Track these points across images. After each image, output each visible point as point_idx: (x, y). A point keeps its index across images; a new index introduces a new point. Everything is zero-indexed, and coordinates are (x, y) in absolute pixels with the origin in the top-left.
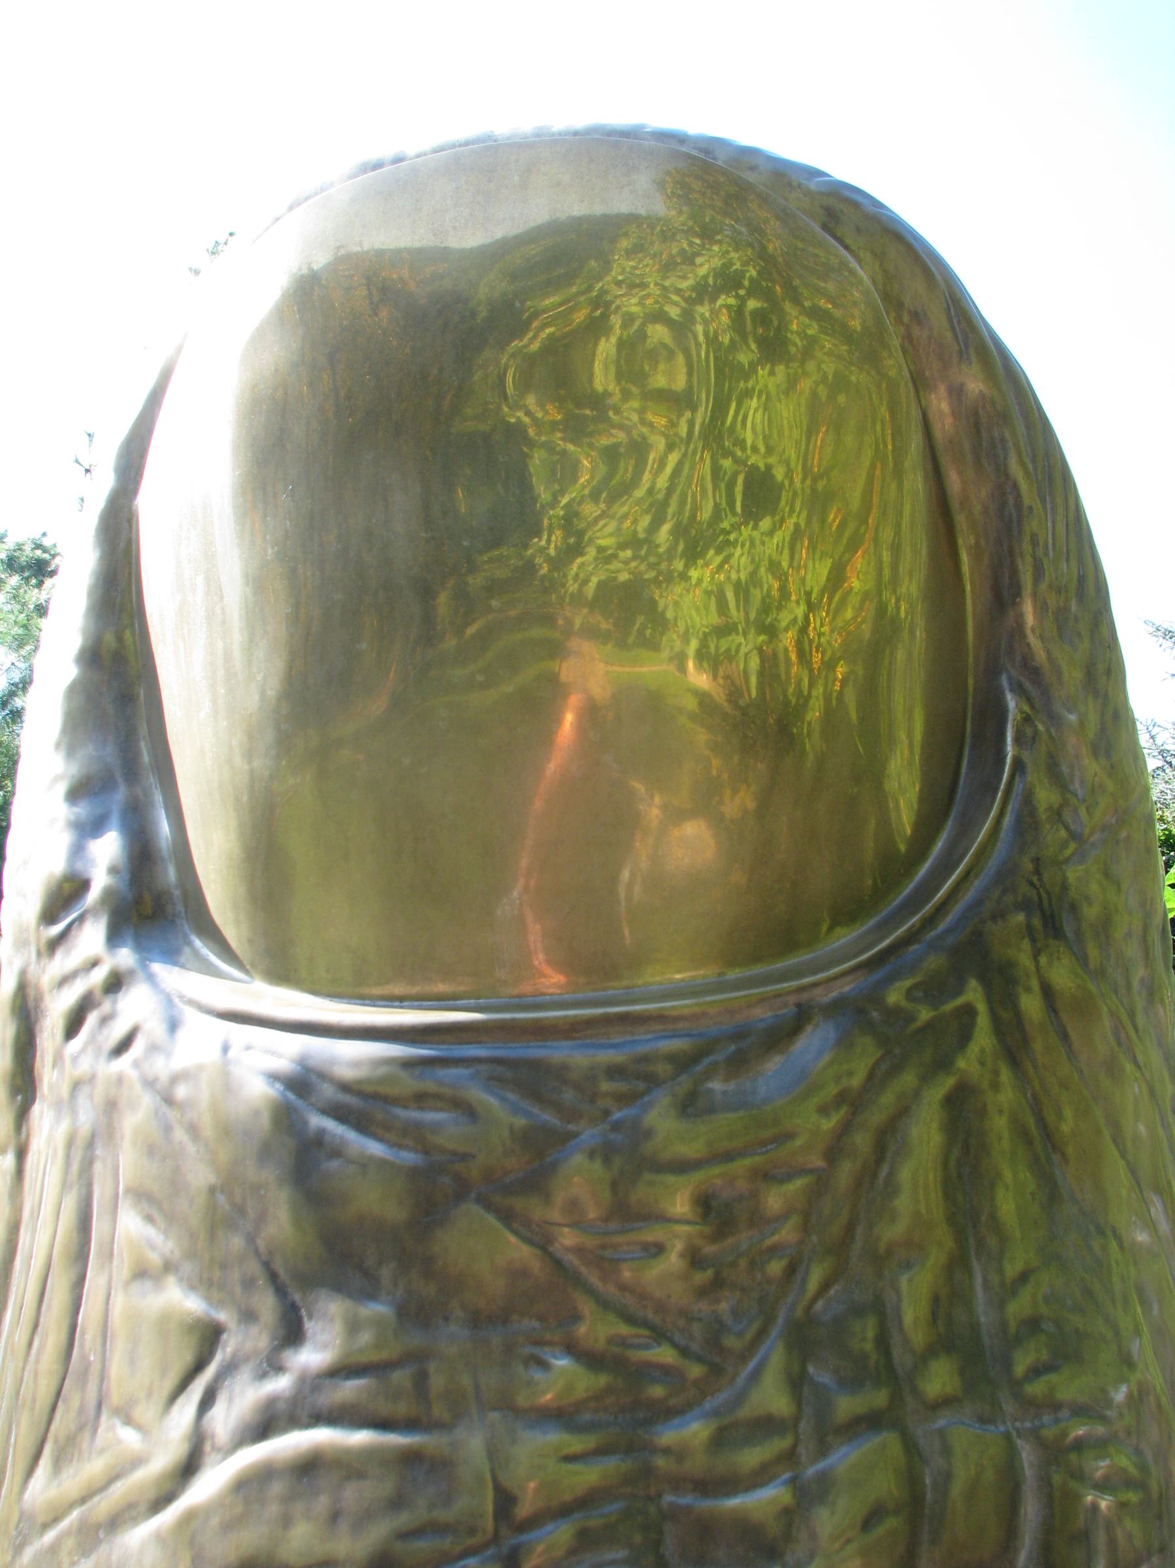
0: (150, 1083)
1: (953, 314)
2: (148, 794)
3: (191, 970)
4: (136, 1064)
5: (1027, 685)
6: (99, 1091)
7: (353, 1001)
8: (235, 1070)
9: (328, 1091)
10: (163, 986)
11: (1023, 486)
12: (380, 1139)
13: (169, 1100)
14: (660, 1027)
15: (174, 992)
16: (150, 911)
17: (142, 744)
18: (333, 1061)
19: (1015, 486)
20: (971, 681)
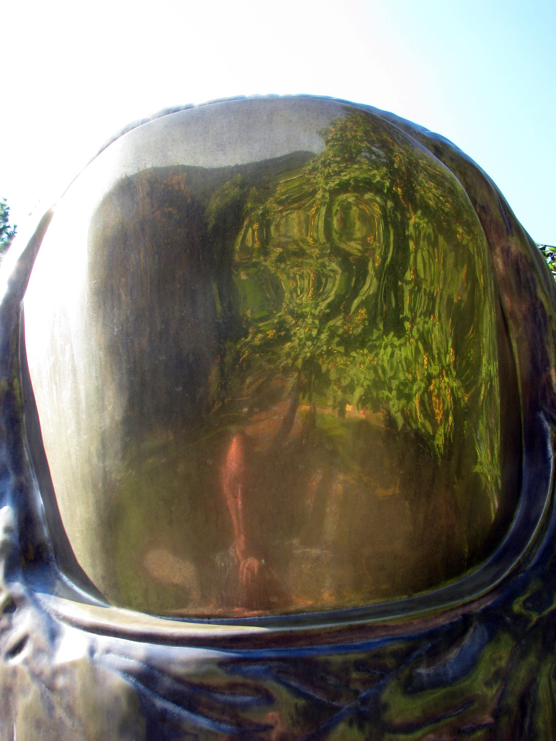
0: (36, 676)
1: (502, 209)
2: (29, 481)
3: (63, 597)
4: (26, 662)
7: (176, 619)
8: (101, 668)
9: (167, 682)
10: (45, 607)
11: (546, 305)
12: (206, 717)
13: (51, 688)
14: (384, 633)
15: (52, 612)
16: (32, 557)
17: (25, 449)
18: (170, 661)
19: (542, 305)
20: (522, 416)
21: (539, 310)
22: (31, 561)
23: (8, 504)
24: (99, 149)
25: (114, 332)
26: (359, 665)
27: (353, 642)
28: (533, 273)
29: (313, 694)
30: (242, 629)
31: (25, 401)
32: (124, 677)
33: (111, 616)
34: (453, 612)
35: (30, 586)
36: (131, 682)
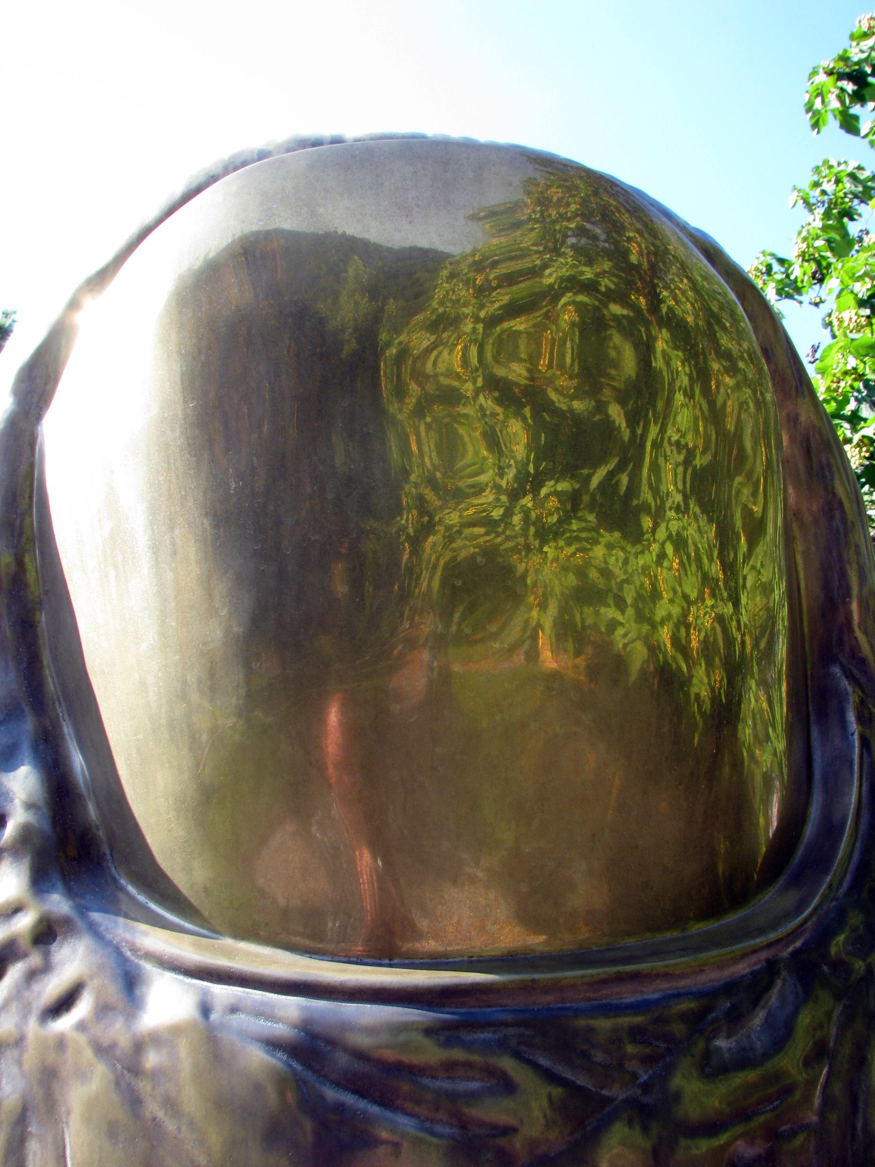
0: (103, 1050)
2: (56, 726)
3: (138, 921)
4: (81, 1026)
5: (856, 672)
6: (31, 1057)
8: (226, 1037)
9: (342, 1059)
10: (109, 936)
12: (411, 1115)
14: (665, 985)
17: (47, 672)
18: (346, 1026)
19: (841, 503)
21: (837, 512)
22: (74, 859)
23: (27, 761)
24: (178, 190)
25: (230, 489)
26: (636, 1034)
27: (621, 998)
28: (830, 456)
29: (573, 1078)
30: (456, 977)
31: (46, 592)
32: (268, 1052)
33: (229, 953)
34: (755, 955)
35: (78, 900)
36: (280, 1059)
